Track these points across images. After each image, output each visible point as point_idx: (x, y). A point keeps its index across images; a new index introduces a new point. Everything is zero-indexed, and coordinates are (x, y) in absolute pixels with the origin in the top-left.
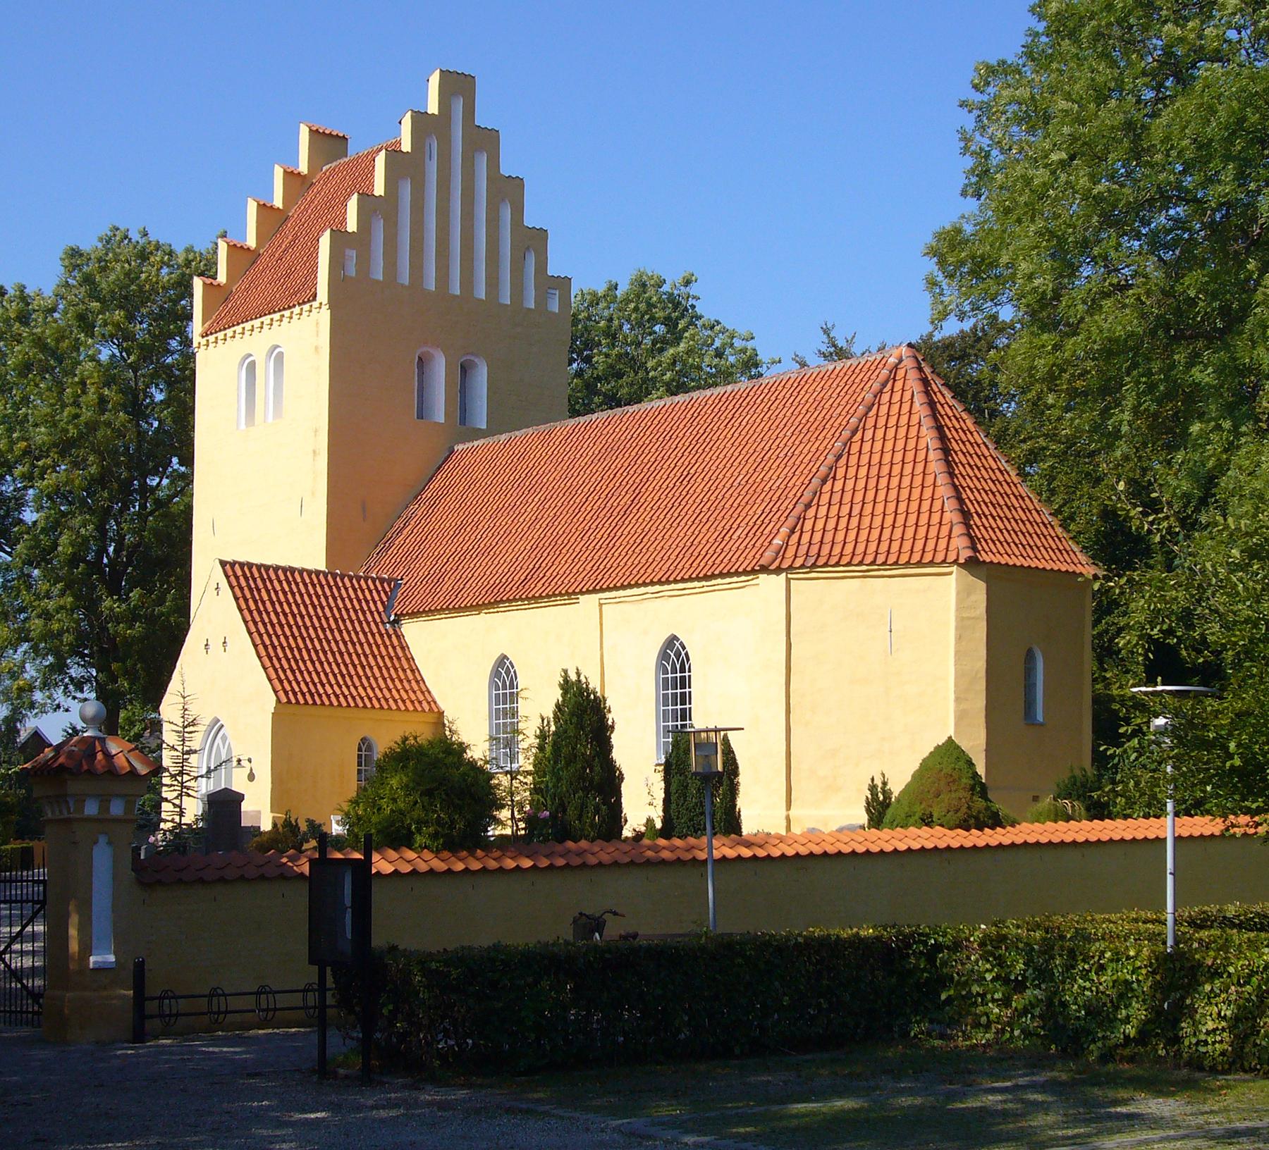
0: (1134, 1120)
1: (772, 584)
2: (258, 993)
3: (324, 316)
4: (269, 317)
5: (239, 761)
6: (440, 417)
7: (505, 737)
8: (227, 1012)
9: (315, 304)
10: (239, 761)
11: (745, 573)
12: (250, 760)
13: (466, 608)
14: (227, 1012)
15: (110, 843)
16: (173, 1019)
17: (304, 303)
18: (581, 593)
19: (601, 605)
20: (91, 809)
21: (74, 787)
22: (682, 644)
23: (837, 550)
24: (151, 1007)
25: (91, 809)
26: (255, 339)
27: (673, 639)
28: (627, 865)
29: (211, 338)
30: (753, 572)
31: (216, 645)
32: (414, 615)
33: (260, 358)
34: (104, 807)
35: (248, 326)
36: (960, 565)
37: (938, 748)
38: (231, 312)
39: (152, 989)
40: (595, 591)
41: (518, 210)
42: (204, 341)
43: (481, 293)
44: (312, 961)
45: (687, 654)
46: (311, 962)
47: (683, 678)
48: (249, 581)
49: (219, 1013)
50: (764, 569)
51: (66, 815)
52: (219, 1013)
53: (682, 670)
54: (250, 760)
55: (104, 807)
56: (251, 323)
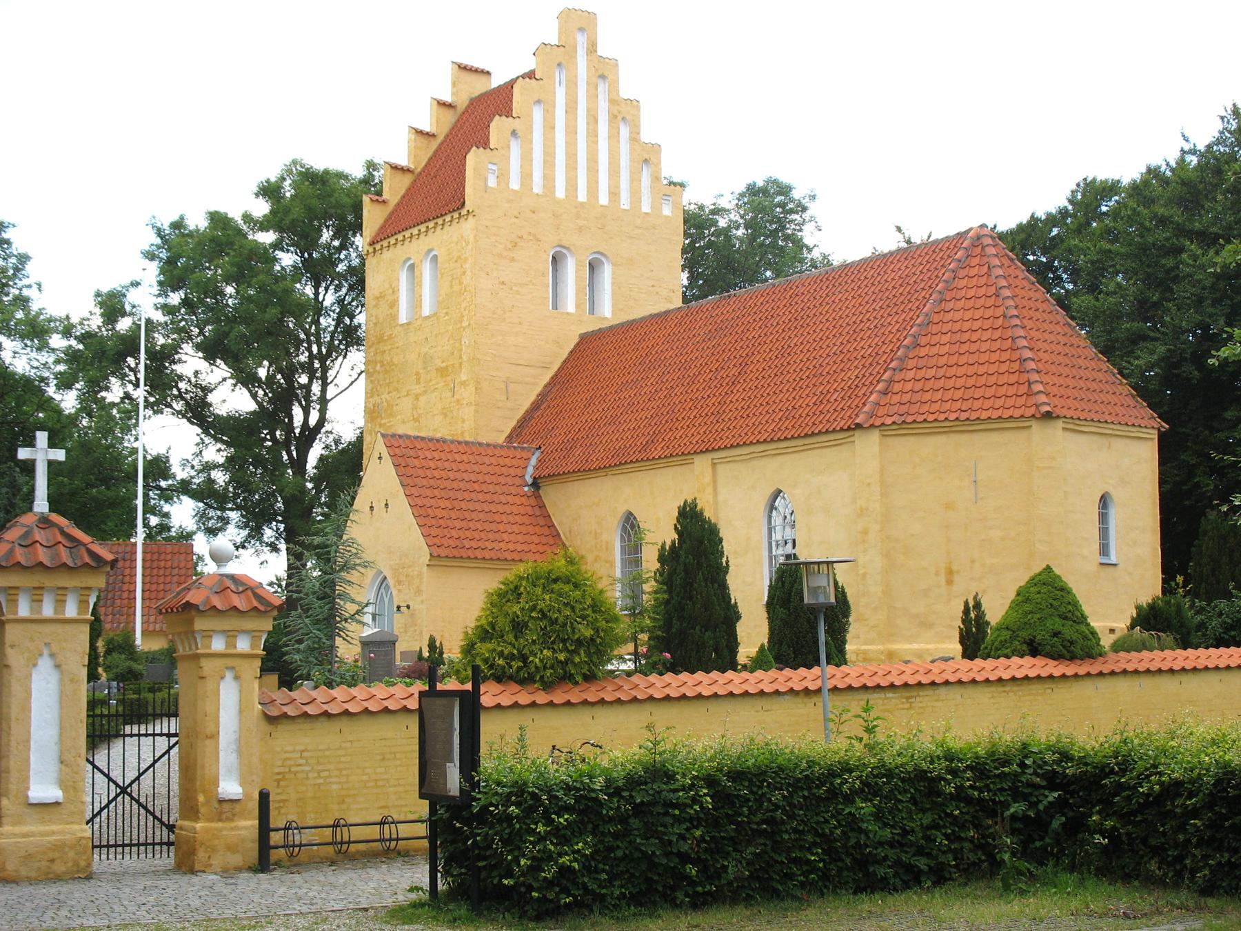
0: (727, 562)
2: (382, 823)
5: (399, 608)
6: (571, 308)
7: (633, 585)
8: (349, 842)
10: (399, 608)
12: (408, 607)
14: (349, 842)
15: (237, 678)
16: (297, 849)
19: (714, 464)
20: (218, 645)
21: (200, 624)
24: (276, 838)
25: (218, 645)
29: (378, 247)
34: (231, 643)
35: (407, 234)
39: (276, 820)
41: (614, 88)
43: (604, 199)
44: (422, 796)
46: (422, 796)
49: (294, 846)
52: (390, 840)
54: (408, 607)
55: (231, 643)
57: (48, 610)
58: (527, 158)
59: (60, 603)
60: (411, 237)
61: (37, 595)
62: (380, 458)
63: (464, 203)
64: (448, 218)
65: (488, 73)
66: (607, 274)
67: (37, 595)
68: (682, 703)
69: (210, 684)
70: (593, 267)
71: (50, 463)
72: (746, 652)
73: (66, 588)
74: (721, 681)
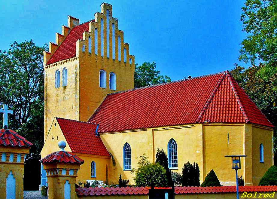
1: (150, 131)
3: (78, 61)
4: (63, 61)
9: (76, 58)
11: (192, 123)
13: (117, 131)
17: (73, 57)
18: (148, 128)
19: (153, 131)
22: (129, 145)
23: (218, 118)
25: (64, 173)
26: (60, 66)
27: (127, 143)
28: (202, 194)
29: (48, 66)
30: (194, 123)
31: (55, 138)
32: (103, 133)
33: (61, 70)
35: (58, 63)
36: (246, 123)
37: (199, 171)
38: (53, 60)
40: (151, 127)
42: (46, 66)
45: (130, 147)
47: (129, 152)
48: (63, 123)
50: (197, 123)
51: (55, 174)
53: (129, 150)
56: (59, 62)
57: (11, 160)
58: (93, 43)
59: (15, 158)
60: (50, 67)
61: (7, 155)
62: (55, 124)
63: (76, 55)
64: (71, 59)
65: (79, 20)
66: (115, 78)
67: (7, 155)
68: (207, 194)
69: (61, 185)
70: (111, 76)
71: (9, 114)
72: (201, 181)
73: (17, 153)
74: (120, 190)
